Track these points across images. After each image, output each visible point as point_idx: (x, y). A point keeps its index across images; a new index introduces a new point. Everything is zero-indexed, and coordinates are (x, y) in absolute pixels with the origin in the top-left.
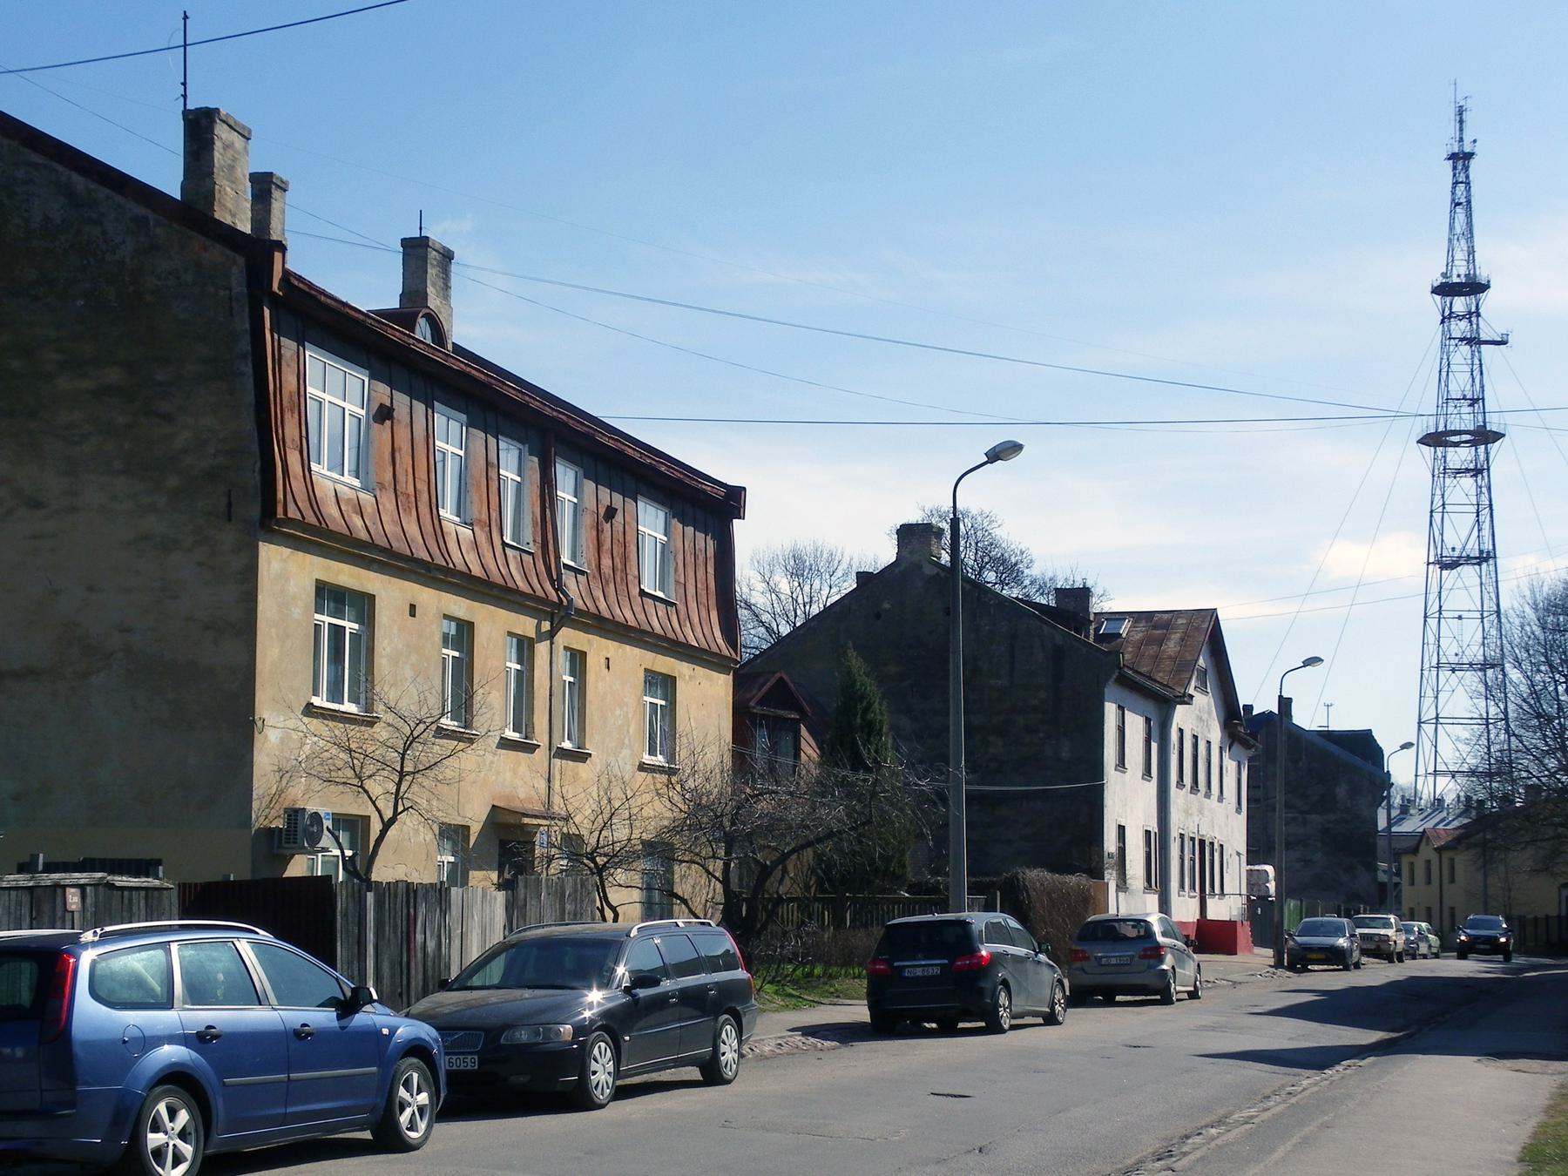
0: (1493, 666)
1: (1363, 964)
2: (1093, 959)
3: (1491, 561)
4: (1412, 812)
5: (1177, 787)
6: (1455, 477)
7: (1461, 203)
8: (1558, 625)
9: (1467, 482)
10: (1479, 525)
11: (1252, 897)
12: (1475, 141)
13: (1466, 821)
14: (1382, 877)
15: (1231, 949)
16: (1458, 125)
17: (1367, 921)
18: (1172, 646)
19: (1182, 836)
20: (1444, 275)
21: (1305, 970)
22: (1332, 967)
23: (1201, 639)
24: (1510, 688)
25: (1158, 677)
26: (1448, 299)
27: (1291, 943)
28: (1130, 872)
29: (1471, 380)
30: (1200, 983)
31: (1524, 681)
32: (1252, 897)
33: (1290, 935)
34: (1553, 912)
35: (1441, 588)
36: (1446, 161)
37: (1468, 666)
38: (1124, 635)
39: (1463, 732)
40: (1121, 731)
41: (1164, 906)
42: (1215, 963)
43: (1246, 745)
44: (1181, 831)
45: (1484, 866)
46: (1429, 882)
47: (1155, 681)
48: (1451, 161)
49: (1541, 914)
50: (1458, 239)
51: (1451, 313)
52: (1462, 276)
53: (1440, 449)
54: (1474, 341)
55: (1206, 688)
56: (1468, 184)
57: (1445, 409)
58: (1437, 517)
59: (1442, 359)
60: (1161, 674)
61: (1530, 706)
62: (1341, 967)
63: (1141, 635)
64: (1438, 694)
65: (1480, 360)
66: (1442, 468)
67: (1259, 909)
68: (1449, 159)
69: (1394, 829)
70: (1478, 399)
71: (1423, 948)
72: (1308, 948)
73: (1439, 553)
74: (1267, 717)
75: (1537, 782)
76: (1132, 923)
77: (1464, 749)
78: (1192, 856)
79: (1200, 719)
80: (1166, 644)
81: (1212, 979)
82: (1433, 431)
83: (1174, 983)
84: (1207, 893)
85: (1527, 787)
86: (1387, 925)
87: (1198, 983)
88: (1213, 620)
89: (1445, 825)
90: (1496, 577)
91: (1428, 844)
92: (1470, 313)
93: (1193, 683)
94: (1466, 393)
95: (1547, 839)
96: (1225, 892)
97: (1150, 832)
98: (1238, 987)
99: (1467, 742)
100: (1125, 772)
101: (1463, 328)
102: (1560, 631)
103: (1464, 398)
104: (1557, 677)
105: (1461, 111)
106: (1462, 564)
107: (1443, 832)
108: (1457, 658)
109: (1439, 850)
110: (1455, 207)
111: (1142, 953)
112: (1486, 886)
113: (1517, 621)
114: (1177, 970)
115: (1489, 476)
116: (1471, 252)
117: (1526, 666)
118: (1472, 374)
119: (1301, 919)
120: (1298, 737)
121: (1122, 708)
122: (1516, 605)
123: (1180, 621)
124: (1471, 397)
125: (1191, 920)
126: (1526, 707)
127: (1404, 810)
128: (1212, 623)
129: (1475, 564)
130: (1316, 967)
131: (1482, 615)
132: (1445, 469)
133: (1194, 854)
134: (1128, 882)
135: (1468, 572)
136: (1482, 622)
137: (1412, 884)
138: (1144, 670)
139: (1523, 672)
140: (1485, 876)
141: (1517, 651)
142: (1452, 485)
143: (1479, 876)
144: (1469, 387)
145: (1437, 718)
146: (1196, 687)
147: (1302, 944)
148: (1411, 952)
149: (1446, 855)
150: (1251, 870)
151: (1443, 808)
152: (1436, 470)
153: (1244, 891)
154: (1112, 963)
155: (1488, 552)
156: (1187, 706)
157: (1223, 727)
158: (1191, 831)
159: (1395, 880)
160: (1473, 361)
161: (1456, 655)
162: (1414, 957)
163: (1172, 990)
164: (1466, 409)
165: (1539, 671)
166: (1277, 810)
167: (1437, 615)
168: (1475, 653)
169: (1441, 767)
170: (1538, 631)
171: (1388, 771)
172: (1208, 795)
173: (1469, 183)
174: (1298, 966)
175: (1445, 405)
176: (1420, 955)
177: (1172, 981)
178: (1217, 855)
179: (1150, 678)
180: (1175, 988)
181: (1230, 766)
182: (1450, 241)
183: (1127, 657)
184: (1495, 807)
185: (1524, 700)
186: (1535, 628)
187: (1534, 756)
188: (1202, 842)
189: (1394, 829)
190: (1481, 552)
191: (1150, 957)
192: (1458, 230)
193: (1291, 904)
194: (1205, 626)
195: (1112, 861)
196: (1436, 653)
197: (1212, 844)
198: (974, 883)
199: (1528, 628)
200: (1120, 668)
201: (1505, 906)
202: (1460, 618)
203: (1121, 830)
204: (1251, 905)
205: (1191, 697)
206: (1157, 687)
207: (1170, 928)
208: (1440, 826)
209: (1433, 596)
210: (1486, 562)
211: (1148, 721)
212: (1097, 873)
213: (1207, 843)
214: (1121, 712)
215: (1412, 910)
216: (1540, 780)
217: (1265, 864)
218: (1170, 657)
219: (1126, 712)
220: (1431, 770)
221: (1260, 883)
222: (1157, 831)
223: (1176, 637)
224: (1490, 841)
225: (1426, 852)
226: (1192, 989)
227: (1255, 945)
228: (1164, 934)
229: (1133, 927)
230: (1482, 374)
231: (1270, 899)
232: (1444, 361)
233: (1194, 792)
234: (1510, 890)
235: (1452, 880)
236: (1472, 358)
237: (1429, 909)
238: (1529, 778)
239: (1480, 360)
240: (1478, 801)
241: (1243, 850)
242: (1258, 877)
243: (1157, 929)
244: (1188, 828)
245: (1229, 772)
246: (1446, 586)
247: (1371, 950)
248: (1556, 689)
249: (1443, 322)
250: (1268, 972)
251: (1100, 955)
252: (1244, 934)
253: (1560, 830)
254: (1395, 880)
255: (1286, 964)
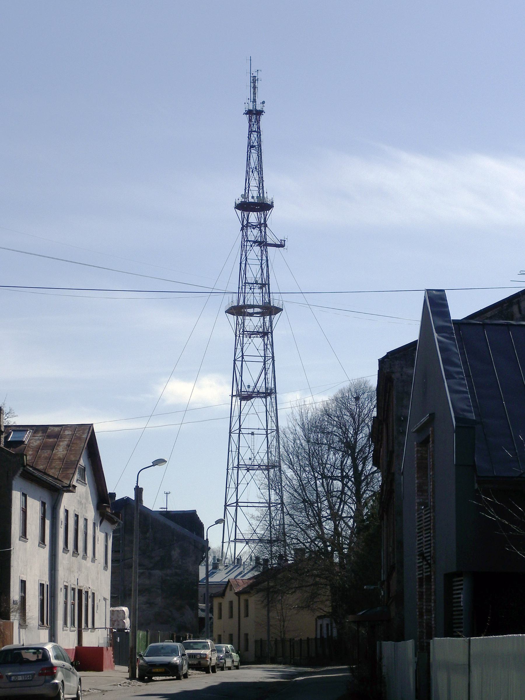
0: (274, 467)
1: (189, 675)
2: (5, 677)
3: (273, 396)
4: (220, 567)
5: (63, 552)
6: (250, 337)
7: (255, 146)
8: (317, 440)
9: (258, 341)
10: (265, 370)
11: (114, 630)
12: (263, 103)
13: (256, 573)
14: (201, 614)
15: (99, 668)
16: (252, 90)
17: (192, 644)
18: (61, 451)
19: (66, 587)
20: (243, 196)
21: (150, 680)
22: (168, 678)
23: (82, 446)
24: (285, 482)
25: (51, 472)
26: (246, 214)
27: (141, 661)
28: (28, 614)
29: (260, 270)
30: (81, 691)
31: (295, 477)
32: (114, 630)
33: (141, 656)
34: (313, 636)
35: (240, 413)
36: (245, 115)
37: (257, 467)
38: (26, 442)
39: (256, 512)
40: (24, 512)
41: (53, 637)
42: (89, 676)
43: (112, 522)
44: (65, 584)
45: (268, 604)
46: (231, 616)
47: (49, 475)
48: (248, 115)
49: (304, 638)
50: (252, 172)
51: (248, 222)
52: (255, 198)
53: (240, 318)
54: (263, 244)
55: (85, 481)
56: (259, 132)
57: (244, 289)
58: (238, 364)
59: (242, 255)
60: (53, 471)
61: (299, 494)
62: (175, 677)
63: (38, 442)
64: (238, 486)
65: (267, 257)
66: (241, 330)
67: (118, 638)
68: (246, 114)
69: (210, 580)
70: (265, 284)
71: (229, 663)
72: (152, 665)
73: (239, 389)
74: (126, 501)
75: (303, 546)
76: (33, 651)
77: (255, 523)
78: (73, 601)
79: (80, 503)
80: (57, 449)
81: (87, 689)
82: (235, 304)
83: (63, 692)
84: (83, 628)
85: (296, 550)
86: (205, 647)
87: (79, 691)
88: (90, 432)
89: (242, 577)
90: (276, 407)
91: (231, 590)
92: (260, 224)
93: (76, 476)
94: (258, 279)
95: (309, 586)
96: (95, 627)
97: (44, 584)
98: (106, 693)
99: (257, 518)
100: (26, 542)
101: (255, 234)
102: (318, 444)
103: (257, 283)
104: (316, 475)
105: (254, 80)
106: (254, 397)
107: (241, 581)
108: (250, 462)
109: (238, 594)
110: (250, 149)
111: (40, 672)
112: (268, 618)
113: (291, 437)
114: (65, 683)
115: (272, 337)
116: (261, 180)
117: (297, 467)
118: (261, 266)
119: (147, 646)
120: (146, 513)
121: (24, 495)
122: (291, 425)
123: (67, 433)
124: (261, 282)
125: (71, 648)
126: (296, 495)
127: (215, 567)
128: (90, 434)
129: (262, 397)
130: (158, 678)
131: (267, 432)
132: (243, 331)
133: (74, 600)
134: (27, 621)
135: (258, 402)
136: (267, 437)
137: (220, 617)
138: (41, 467)
139: (295, 471)
140: (269, 611)
141: (291, 457)
142: (248, 342)
143: (264, 612)
144: (259, 275)
145: (237, 502)
146: (77, 480)
147: (149, 662)
148: (221, 665)
149: (243, 597)
150: (113, 611)
151: (241, 565)
152: (238, 332)
153: (108, 626)
154: (19, 679)
155: (271, 389)
156: (72, 493)
157: (96, 509)
158: (72, 583)
159: (210, 615)
160: (262, 258)
161: (250, 459)
162: (222, 669)
163: (62, 697)
164: (257, 290)
165: (305, 471)
166: (133, 567)
167: (238, 431)
168: (262, 458)
169: (239, 536)
170: (304, 443)
171: (207, 539)
172: (85, 557)
173: (260, 132)
174: (146, 678)
175: (244, 287)
176: (226, 667)
177: (61, 691)
178: (90, 600)
179: (45, 473)
180: (63, 696)
181: (100, 536)
182: (247, 173)
183: (28, 458)
184: (275, 564)
185: (296, 491)
186: (302, 441)
187: (301, 528)
188: (80, 591)
189: (210, 580)
190: (267, 389)
191: (46, 674)
192: (252, 165)
193: (141, 634)
194: (85, 436)
195: (17, 607)
196: (236, 458)
197: (87, 592)
198: (193, 638)
199: (298, 442)
200: (24, 466)
201: (281, 632)
202: (253, 434)
203: (23, 583)
204: (113, 636)
205: (74, 487)
206: (50, 479)
207: (60, 653)
208: (239, 577)
209: (235, 419)
210: (270, 396)
211: (43, 504)
212: (5, 615)
213: (83, 592)
214: (24, 498)
215: (220, 636)
216: (304, 545)
217: (123, 606)
218: (60, 459)
219: (28, 498)
220: (232, 538)
221: (119, 619)
222: (48, 584)
223: (63, 444)
224: (272, 587)
225: (230, 596)
226: (75, 696)
227: (115, 664)
228: (57, 657)
229: (34, 653)
230: (268, 266)
231: (126, 631)
232: (243, 256)
233: (75, 555)
234: (284, 622)
235: (247, 615)
236: (262, 256)
237: (231, 636)
238: (298, 544)
239: (267, 257)
240: (264, 560)
241: (108, 596)
242: (118, 616)
243: (51, 654)
244: (70, 581)
245: (100, 541)
246: (244, 412)
247: (195, 664)
248: (316, 483)
249: (242, 229)
250: (125, 683)
251: (10, 674)
252: (108, 656)
253: (318, 579)
254: (210, 615)
255: (137, 677)
